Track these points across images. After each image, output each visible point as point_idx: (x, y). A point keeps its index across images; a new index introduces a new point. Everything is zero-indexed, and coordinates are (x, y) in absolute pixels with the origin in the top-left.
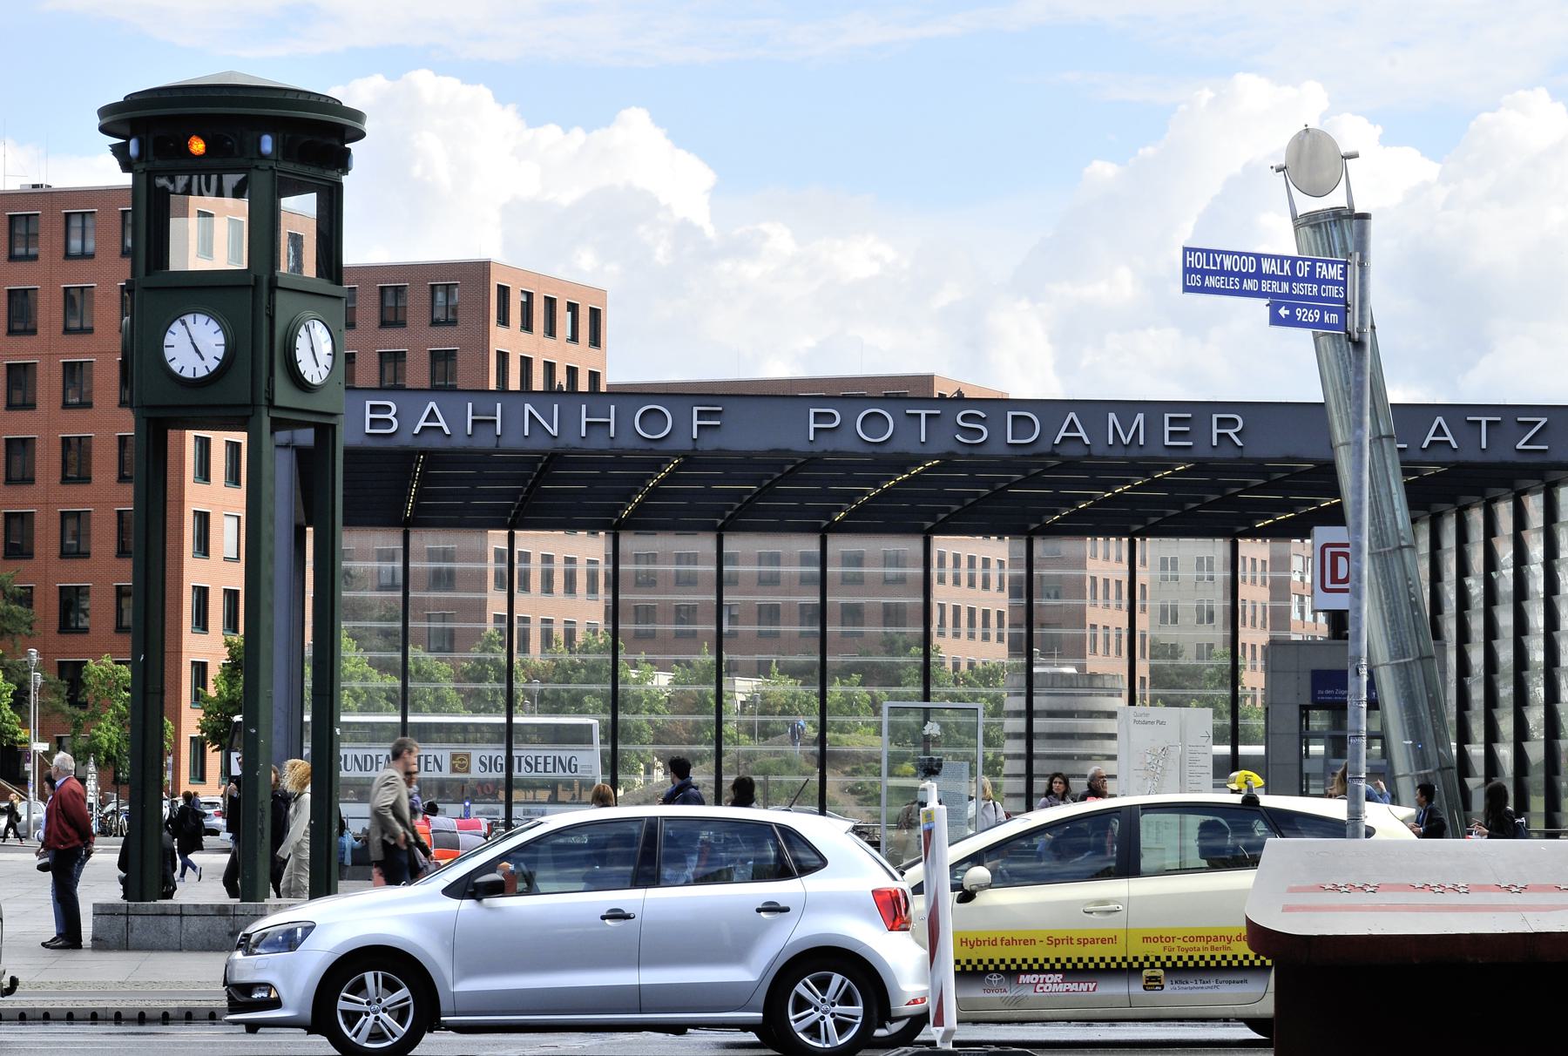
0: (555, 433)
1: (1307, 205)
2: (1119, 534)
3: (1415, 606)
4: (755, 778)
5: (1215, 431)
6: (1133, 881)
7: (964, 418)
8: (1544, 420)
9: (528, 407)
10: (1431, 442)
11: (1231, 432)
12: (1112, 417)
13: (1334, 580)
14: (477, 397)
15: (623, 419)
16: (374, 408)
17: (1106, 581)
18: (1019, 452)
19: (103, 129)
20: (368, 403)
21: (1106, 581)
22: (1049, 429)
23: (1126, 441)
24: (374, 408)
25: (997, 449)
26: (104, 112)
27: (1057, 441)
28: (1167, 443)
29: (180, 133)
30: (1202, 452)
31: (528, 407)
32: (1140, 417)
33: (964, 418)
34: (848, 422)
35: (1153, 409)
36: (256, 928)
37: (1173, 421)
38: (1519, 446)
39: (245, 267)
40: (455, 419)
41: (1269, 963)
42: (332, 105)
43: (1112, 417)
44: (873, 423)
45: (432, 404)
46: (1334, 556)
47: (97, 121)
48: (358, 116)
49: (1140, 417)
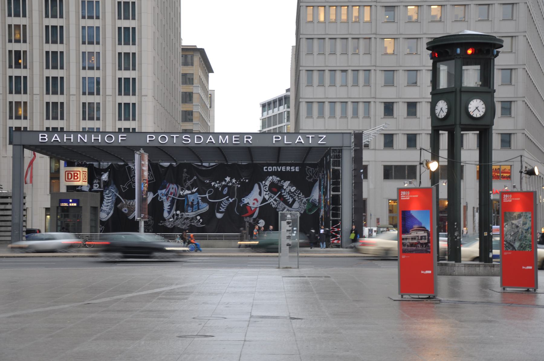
0: (86, 141)
5: (245, 140)
7: (185, 137)
8: (325, 136)
9: (79, 135)
11: (249, 140)
12: (220, 137)
13: (68, 179)
15: (103, 139)
16: (42, 136)
18: (321, 146)
19: (428, 49)
32: (227, 137)
33: (185, 137)
37: (235, 137)
38: (319, 142)
39: (446, 132)
41: (201, 220)
42: (494, 38)
43: (220, 137)
44: (163, 138)
45: (56, 135)
46: (68, 173)
49: (227, 137)
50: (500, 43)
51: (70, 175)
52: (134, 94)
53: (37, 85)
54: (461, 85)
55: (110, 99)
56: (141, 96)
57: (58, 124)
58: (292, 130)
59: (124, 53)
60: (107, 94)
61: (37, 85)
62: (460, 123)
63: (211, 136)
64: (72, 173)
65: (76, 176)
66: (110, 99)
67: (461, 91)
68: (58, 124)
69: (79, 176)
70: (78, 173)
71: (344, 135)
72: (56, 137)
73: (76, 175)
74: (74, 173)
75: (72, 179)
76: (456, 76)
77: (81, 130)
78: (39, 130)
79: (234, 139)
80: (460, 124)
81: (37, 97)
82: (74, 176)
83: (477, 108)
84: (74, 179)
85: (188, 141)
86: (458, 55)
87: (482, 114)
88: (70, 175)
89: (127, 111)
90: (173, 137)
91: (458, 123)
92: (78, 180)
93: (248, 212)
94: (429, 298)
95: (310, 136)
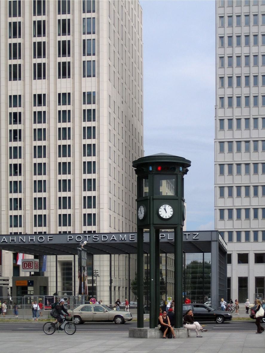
0: (25, 241)
7: (95, 236)
8: (198, 234)
9: (20, 237)
10: (112, 239)
13: (25, 267)
14: (25, 236)
20: (68, 236)
23: (123, 239)
25: (100, 242)
26: (134, 162)
27: (111, 240)
28: (130, 239)
31: (20, 237)
32: (125, 235)
33: (95, 236)
36: (84, 323)
37: (49, 237)
38: (194, 238)
42: (184, 159)
46: (25, 263)
47: (191, 164)
48: (190, 162)
49: (125, 235)
50: (189, 163)
51: (26, 264)
52: (70, 208)
53: (28, 204)
55: (77, 211)
56: (99, 208)
57: (43, 229)
59: (88, 179)
60: (76, 208)
61: (28, 204)
62: (153, 223)
63: (113, 235)
64: (27, 263)
65: (30, 265)
66: (77, 211)
67: (153, 199)
68: (43, 229)
69: (32, 265)
70: (31, 263)
71: (213, 232)
72: (4, 239)
73: (30, 264)
74: (29, 263)
75: (27, 268)
76: (155, 188)
77: (58, 233)
78: (79, 233)
79: (130, 237)
80: (153, 224)
81: (28, 212)
82: (29, 265)
84: (29, 267)
85: (97, 239)
86: (151, 171)
88: (26, 264)
89: (90, 219)
90: (186, 234)
91: (152, 223)
92: (32, 268)
95: (87, 236)
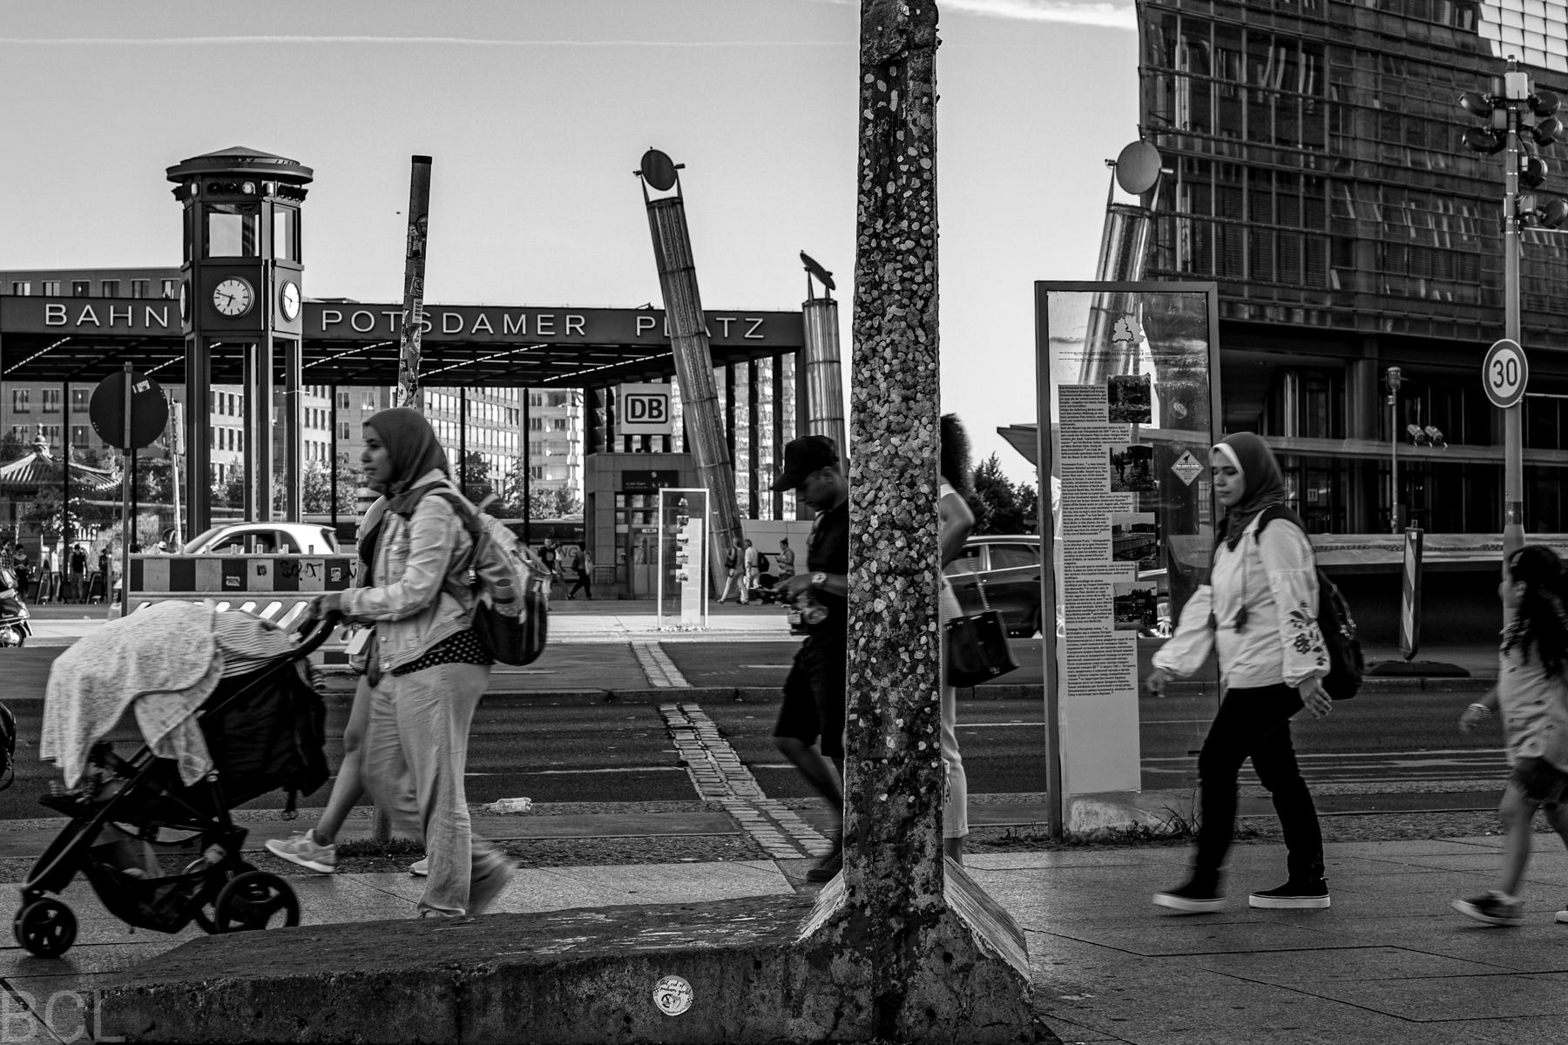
1: (655, 194)
2: (455, 385)
3: (718, 424)
4: (1107, 424)
6: (47, 706)
12: (506, 317)
13: (633, 416)
16: (51, 309)
17: (231, 432)
19: (169, 179)
21: (231, 432)
22: (469, 324)
24: (51, 309)
29: (214, 182)
30: (560, 339)
34: (346, 319)
35: (532, 312)
40: (103, 316)
43: (506, 317)
46: (633, 401)
51: (638, 405)
54: (206, 251)
58: (1160, 220)
64: (646, 399)
65: (657, 408)
69: (663, 408)
72: (482, 323)
75: (646, 418)
82: (651, 408)
83: (231, 298)
84: (651, 416)
87: (228, 313)
88: (638, 405)
92: (663, 418)
93: (1402, 566)
94: (1502, 926)
